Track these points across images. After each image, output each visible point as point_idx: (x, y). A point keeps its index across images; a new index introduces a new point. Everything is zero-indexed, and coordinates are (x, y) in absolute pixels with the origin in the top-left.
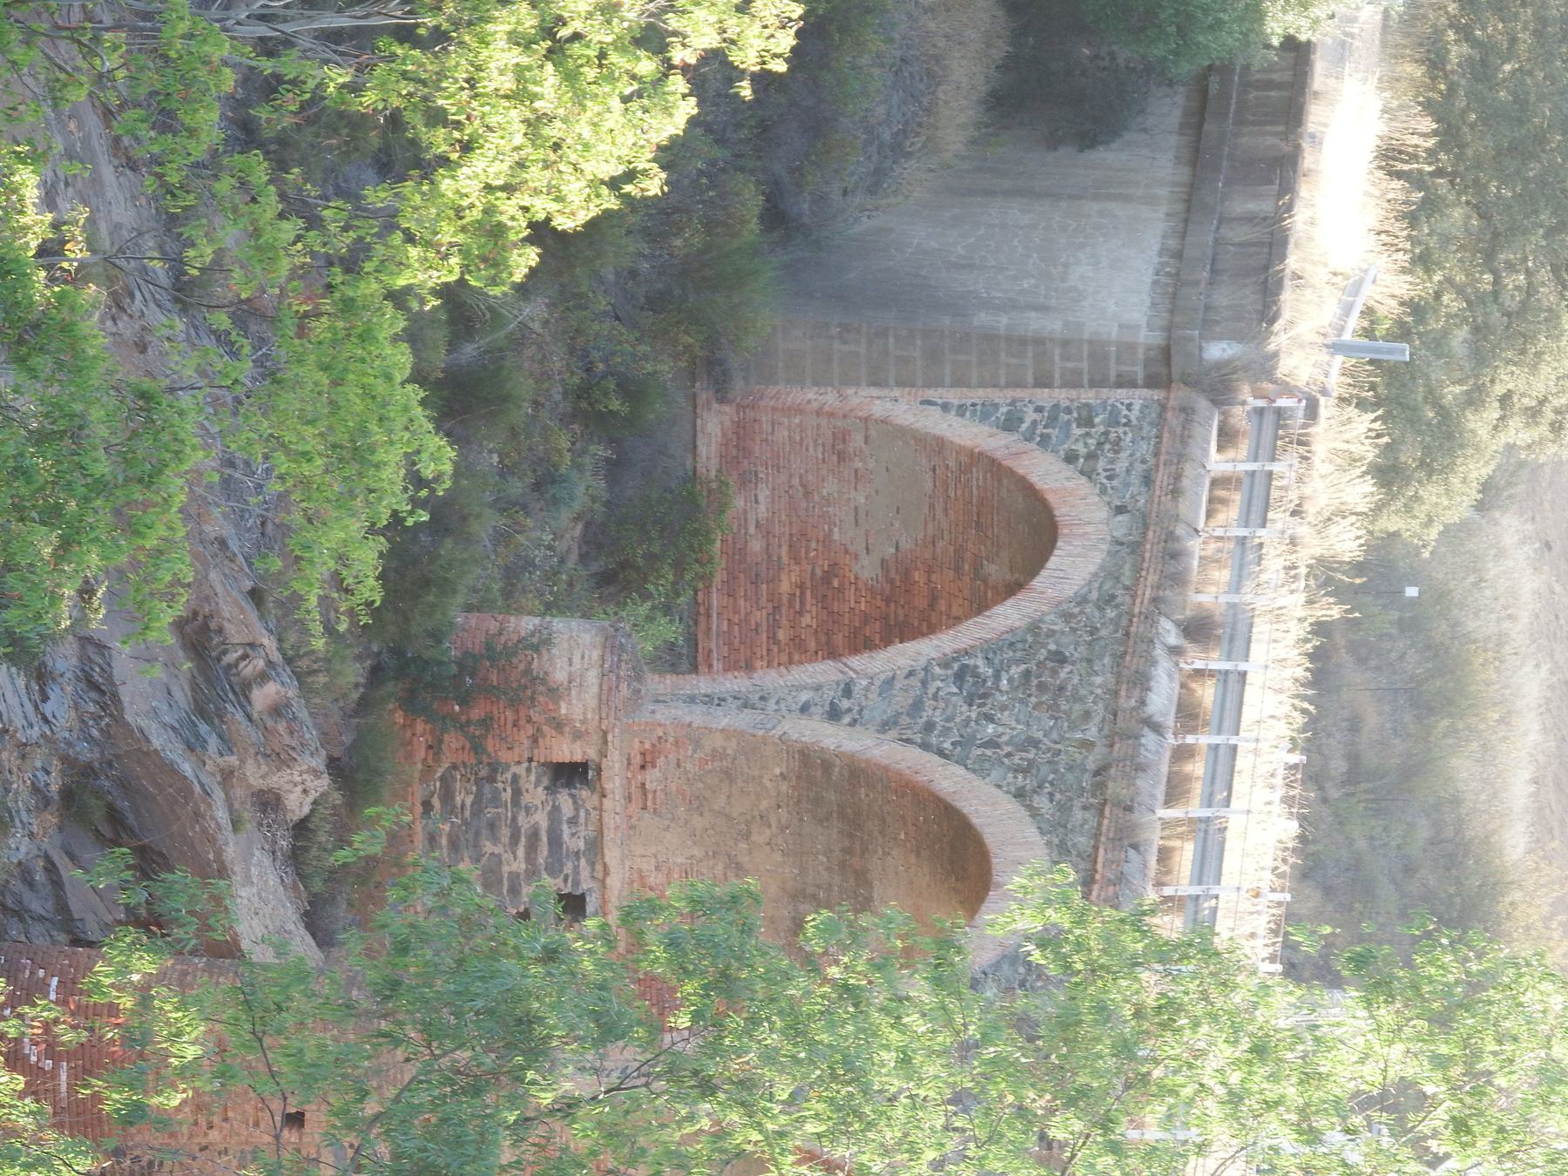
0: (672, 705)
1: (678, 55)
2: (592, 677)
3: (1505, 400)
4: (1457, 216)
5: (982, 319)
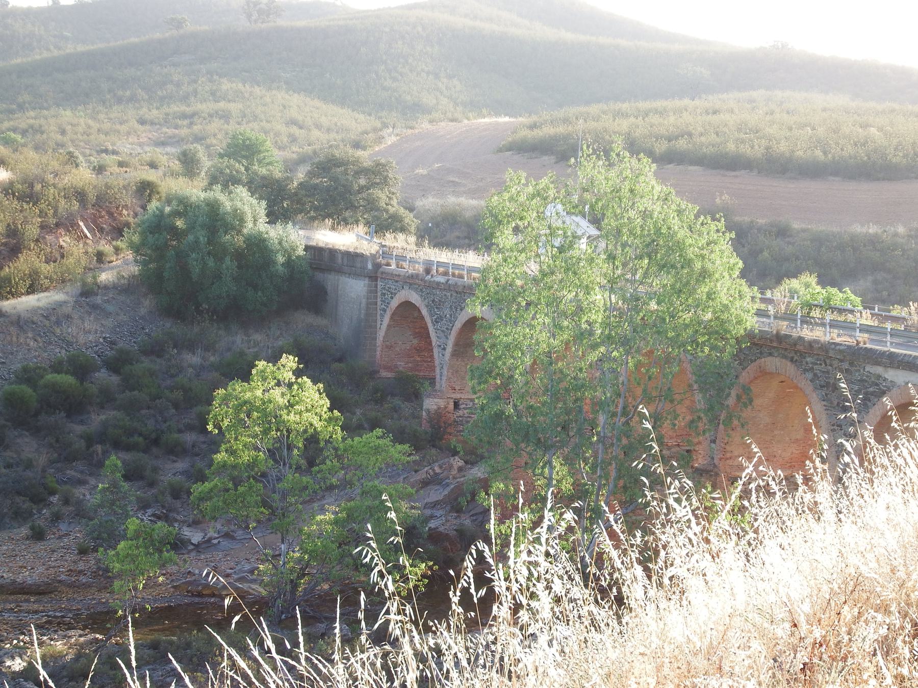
0: (442, 383)
1: (293, 380)
2: (436, 400)
3: (387, 204)
4: (347, 214)
5: (362, 316)
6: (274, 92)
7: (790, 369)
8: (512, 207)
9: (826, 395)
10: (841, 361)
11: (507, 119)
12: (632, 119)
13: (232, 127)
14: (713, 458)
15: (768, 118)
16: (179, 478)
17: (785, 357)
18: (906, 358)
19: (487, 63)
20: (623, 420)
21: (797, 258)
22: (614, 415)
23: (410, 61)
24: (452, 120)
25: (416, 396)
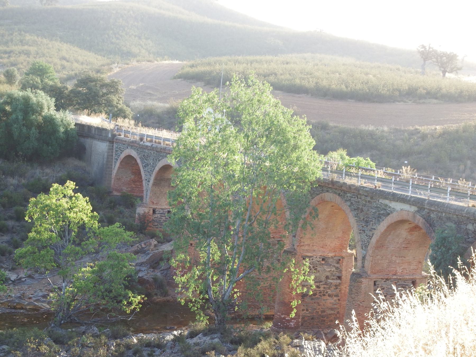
1: (73, 195)
3: (117, 103)
5: (105, 162)
6: (54, 42)
7: (338, 199)
8: (195, 107)
9: (357, 214)
10: (366, 196)
12: (245, 65)
13: (31, 60)
14: (294, 245)
15: (316, 67)
16: (4, 245)
17: (336, 193)
18: (402, 197)
19: (168, 33)
20: (249, 223)
21: (332, 141)
22: (244, 220)
23: (126, 29)
24: (149, 61)
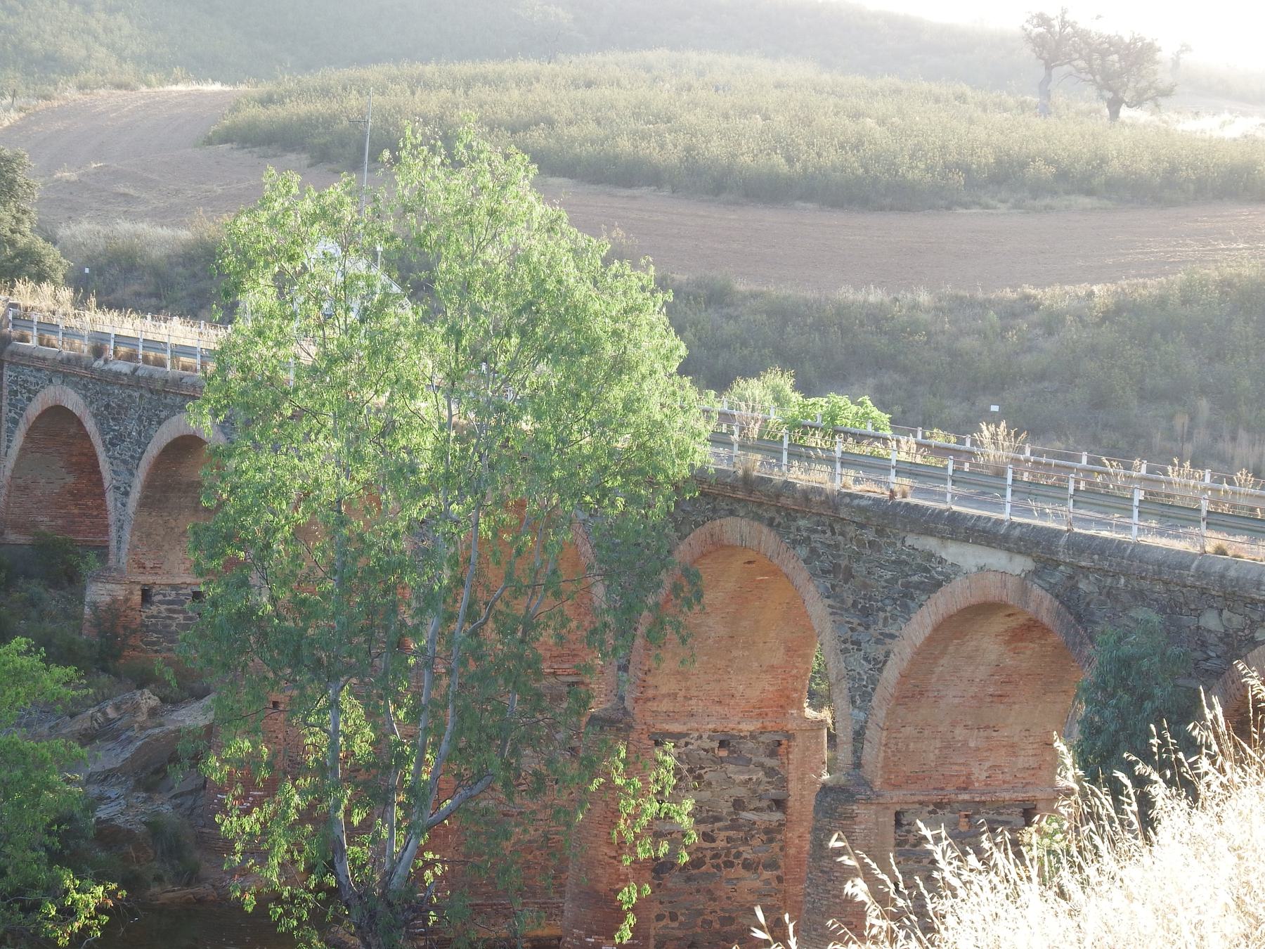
0: (121, 556)
2: (108, 586)
3: (13, 232)
7: (768, 540)
9: (833, 587)
10: (862, 526)
11: (217, 87)
12: (445, 93)
14: (622, 698)
17: (759, 518)
18: (981, 524)
20: (468, 627)
21: (744, 344)
22: (451, 617)
24: (119, 86)
25: (68, 578)
